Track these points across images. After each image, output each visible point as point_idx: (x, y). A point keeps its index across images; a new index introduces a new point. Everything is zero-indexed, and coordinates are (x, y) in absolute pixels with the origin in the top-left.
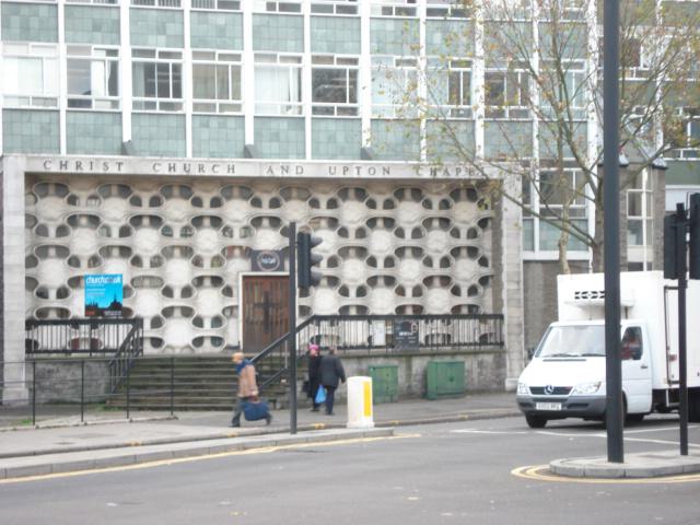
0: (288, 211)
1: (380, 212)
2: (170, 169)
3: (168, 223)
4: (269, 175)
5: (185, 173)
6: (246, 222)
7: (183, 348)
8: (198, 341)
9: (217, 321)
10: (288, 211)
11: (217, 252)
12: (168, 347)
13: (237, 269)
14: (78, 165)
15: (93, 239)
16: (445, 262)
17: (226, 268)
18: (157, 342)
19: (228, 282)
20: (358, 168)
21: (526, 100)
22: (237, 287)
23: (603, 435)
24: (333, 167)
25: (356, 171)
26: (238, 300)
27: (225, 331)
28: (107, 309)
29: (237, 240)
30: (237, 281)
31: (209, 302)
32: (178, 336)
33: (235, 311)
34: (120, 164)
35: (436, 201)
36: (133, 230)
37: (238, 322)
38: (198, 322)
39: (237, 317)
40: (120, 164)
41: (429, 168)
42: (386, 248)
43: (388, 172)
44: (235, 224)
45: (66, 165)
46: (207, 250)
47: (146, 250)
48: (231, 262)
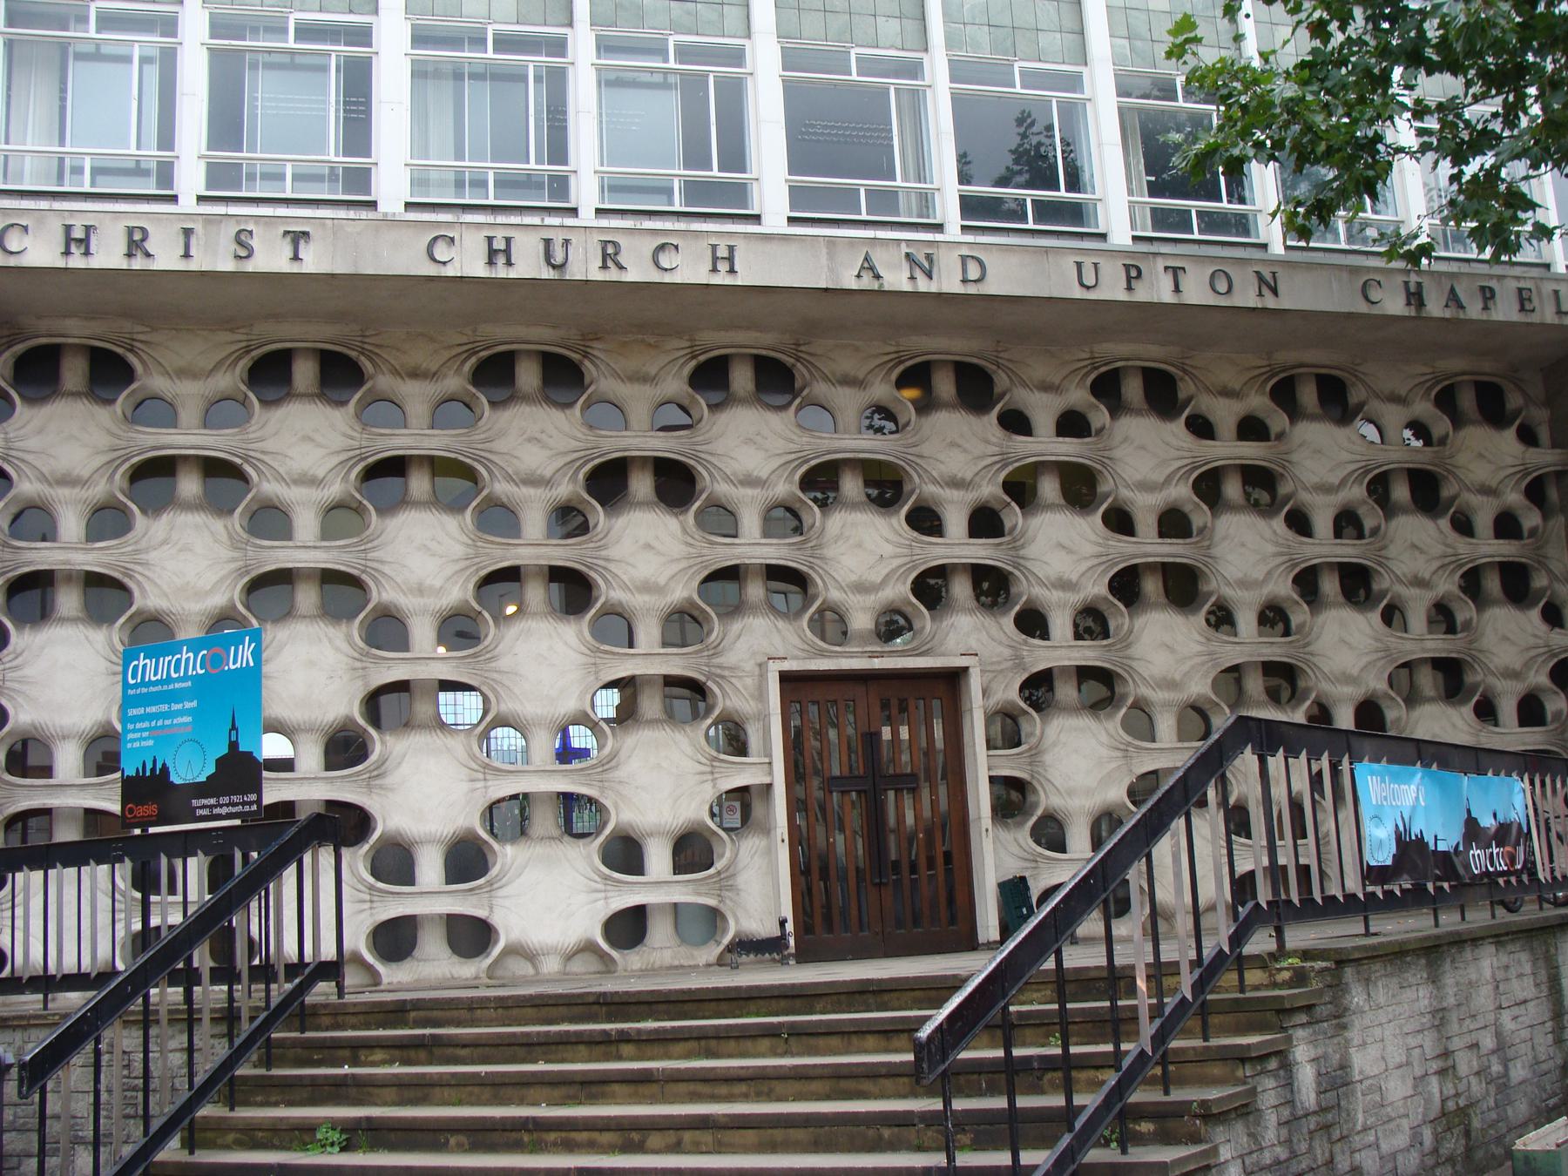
0: (925, 449)
1: (1046, 445)
2: (492, 255)
3: (269, 488)
4: (867, 283)
5: (547, 274)
6: (568, 488)
7: (569, 957)
8: (628, 927)
9: (692, 851)
10: (925, 449)
11: (683, 591)
12: (514, 950)
13: (757, 653)
14: (136, 243)
15: (225, 553)
16: (1091, 622)
17: (717, 650)
18: (471, 935)
19: (732, 698)
20: (1175, 272)
21: (1342, 46)
22: (764, 717)
23: (181, 989)
24: (1088, 262)
25: (1166, 282)
26: (767, 765)
27: (726, 883)
28: (201, 790)
29: (305, 549)
30: (761, 695)
31: (661, 781)
32: (549, 906)
33: (757, 809)
34: (298, 238)
35: (1043, 410)
36: (598, 515)
37: (770, 852)
38: (625, 855)
39: (767, 830)
40: (298, 238)
41: (1400, 279)
42: (210, 578)
43: (1275, 292)
44: (64, 492)
45: (85, 242)
46: (647, 587)
47: (420, 590)
48: (736, 626)
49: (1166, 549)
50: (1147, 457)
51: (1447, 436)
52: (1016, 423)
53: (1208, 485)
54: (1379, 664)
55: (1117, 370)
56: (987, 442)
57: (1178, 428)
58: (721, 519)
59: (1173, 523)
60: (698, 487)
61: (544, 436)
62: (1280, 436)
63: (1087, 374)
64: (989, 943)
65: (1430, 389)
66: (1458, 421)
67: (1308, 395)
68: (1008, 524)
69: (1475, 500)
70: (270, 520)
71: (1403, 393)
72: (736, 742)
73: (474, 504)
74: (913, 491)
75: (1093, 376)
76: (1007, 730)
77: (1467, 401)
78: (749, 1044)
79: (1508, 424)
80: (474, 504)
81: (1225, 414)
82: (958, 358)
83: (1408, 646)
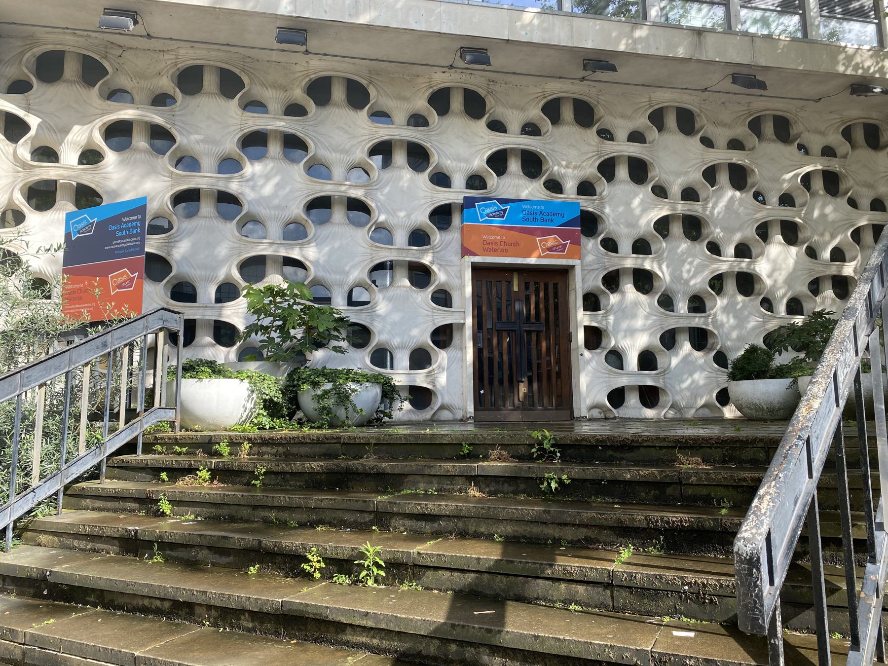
29: (206, 180)
30: (461, 277)
49: (783, 213)
50: (678, 159)
51: (847, 154)
52: (606, 134)
53: (710, 175)
54: (804, 277)
55: (662, 108)
56: (590, 145)
57: (695, 141)
58: (187, 162)
59: (689, 194)
60: (544, 168)
61: (345, 126)
62: (845, 157)
63: (646, 110)
64: (646, 419)
65: (839, 127)
66: (853, 147)
67: (768, 129)
68: (598, 190)
69: (864, 191)
70: (317, 169)
71: (823, 129)
72: (443, 298)
73: (305, 160)
74: (548, 170)
75: (650, 111)
76: (592, 302)
77: (859, 135)
78: (132, 473)
79: (792, 142)
80: (305, 160)
81: (721, 136)
82: (775, 113)
83: (820, 268)
